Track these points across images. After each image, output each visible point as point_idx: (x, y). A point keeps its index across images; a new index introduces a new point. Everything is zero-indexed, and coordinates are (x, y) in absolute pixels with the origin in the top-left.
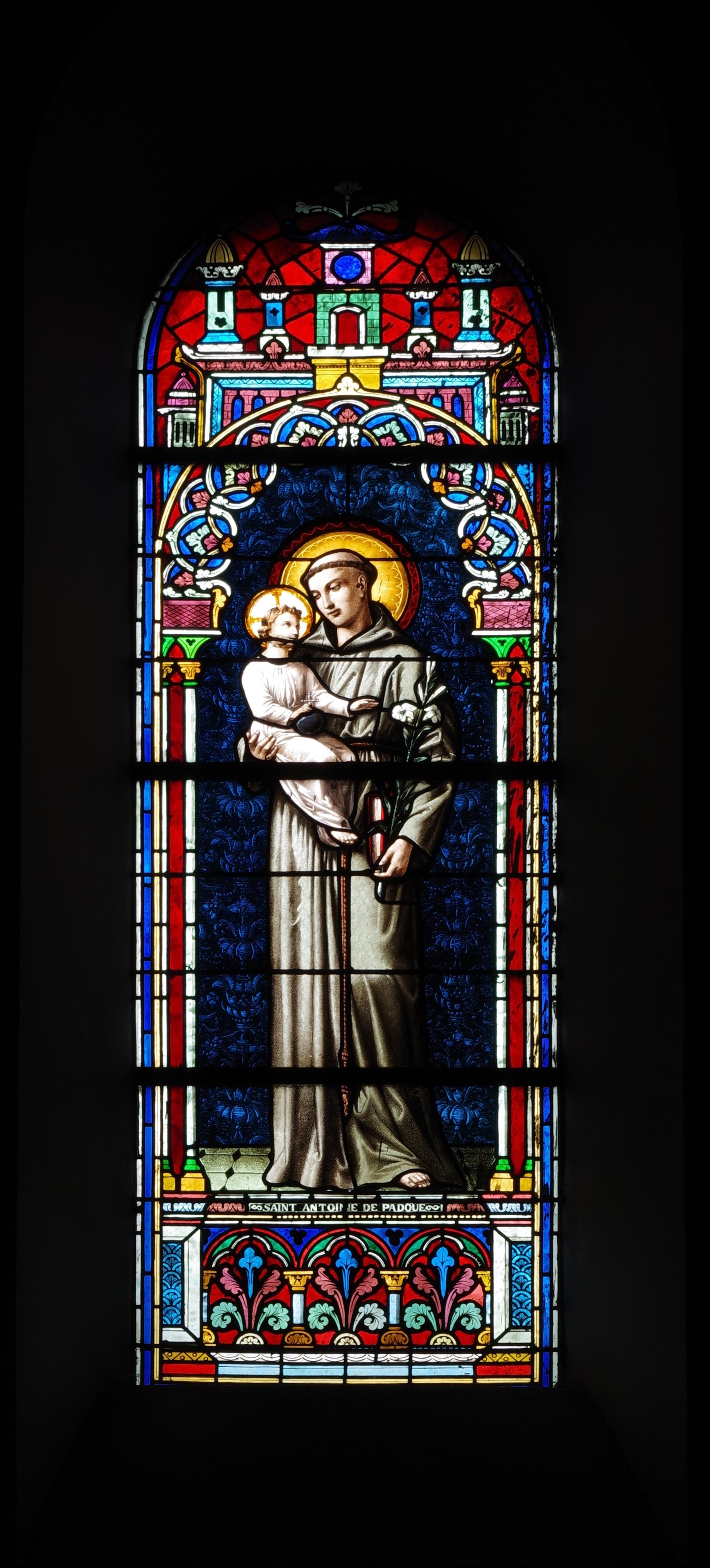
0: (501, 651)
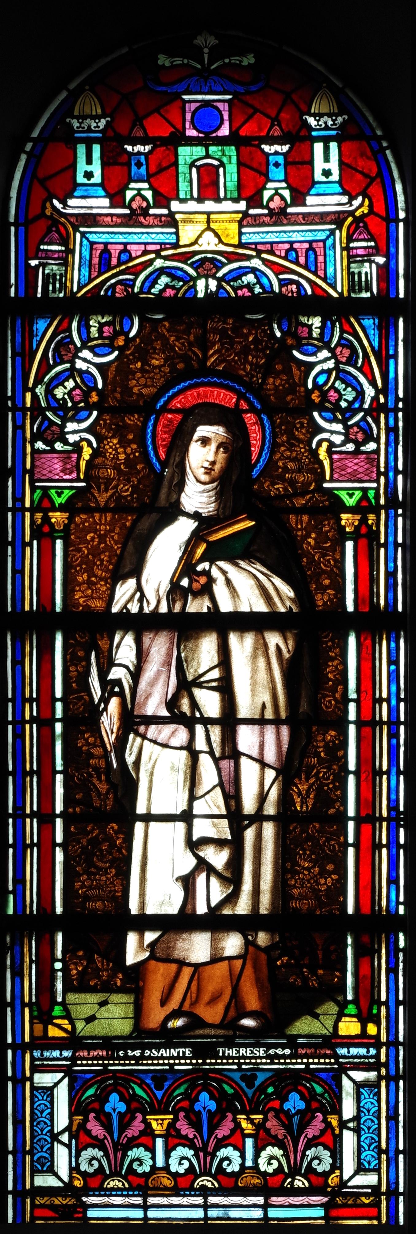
0: (350, 502)
